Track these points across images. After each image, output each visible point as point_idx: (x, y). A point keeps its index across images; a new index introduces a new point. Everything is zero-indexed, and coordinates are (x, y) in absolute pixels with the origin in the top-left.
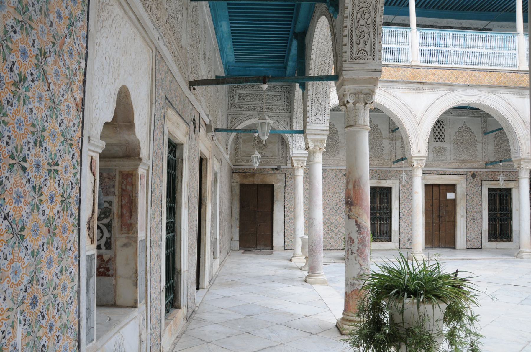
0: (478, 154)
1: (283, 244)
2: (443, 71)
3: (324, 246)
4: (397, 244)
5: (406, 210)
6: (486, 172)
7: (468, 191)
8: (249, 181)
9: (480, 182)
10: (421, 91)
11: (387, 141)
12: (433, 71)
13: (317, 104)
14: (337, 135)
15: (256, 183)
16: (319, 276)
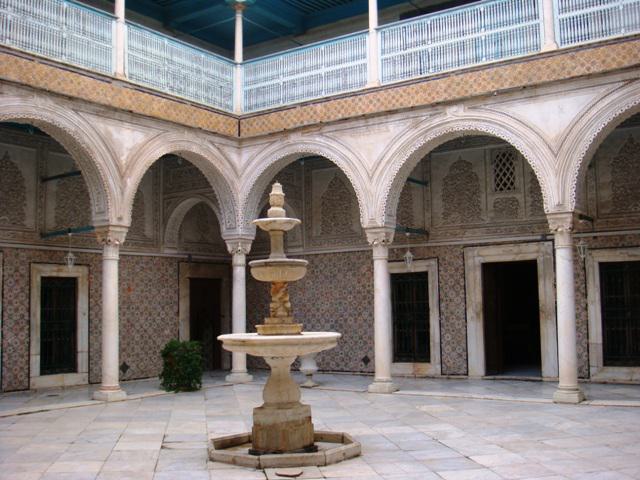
4: (439, 367)
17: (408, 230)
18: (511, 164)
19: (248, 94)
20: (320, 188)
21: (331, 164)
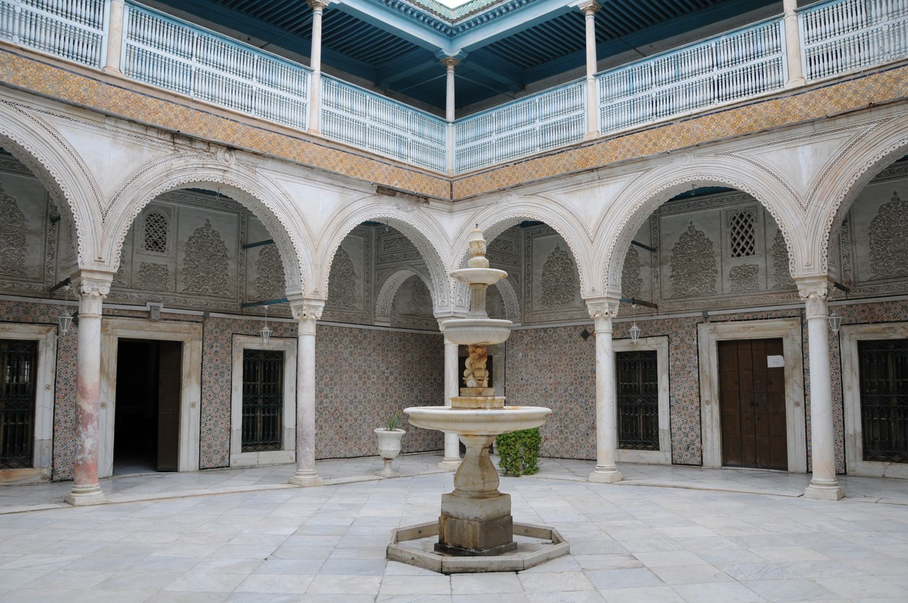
3: (317, 451)
4: (669, 455)
5: (681, 392)
6: (851, 306)
11: (647, 268)
12: (615, 142)
17: (634, 301)
18: (750, 226)
19: (460, 155)
20: (541, 260)
21: (551, 231)
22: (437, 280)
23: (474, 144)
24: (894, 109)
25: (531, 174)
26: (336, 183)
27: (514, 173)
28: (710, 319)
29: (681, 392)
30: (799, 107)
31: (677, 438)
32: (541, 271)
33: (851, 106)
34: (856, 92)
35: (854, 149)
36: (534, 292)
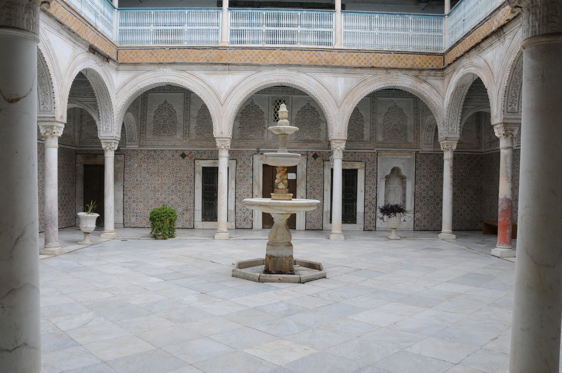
0: (321, 133)
1: (122, 222)
2: (251, 51)
4: (233, 224)
5: (242, 191)
7: (309, 172)
8: (89, 162)
9: (322, 162)
10: (227, 72)
12: (240, 51)
13: (43, 94)
14: (176, 117)
15: (98, 163)
16: (50, 247)
22: (104, 114)
23: (135, 28)
24: (379, 71)
25: (181, 57)
26: (72, 39)
27: (169, 55)
28: (260, 152)
29: (242, 191)
30: (340, 59)
31: (238, 215)
32: (153, 115)
33: (363, 65)
34: (365, 58)
35: (362, 84)
36: (147, 127)
